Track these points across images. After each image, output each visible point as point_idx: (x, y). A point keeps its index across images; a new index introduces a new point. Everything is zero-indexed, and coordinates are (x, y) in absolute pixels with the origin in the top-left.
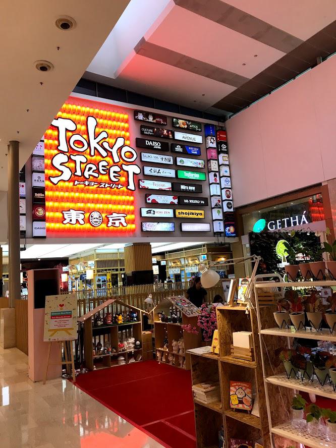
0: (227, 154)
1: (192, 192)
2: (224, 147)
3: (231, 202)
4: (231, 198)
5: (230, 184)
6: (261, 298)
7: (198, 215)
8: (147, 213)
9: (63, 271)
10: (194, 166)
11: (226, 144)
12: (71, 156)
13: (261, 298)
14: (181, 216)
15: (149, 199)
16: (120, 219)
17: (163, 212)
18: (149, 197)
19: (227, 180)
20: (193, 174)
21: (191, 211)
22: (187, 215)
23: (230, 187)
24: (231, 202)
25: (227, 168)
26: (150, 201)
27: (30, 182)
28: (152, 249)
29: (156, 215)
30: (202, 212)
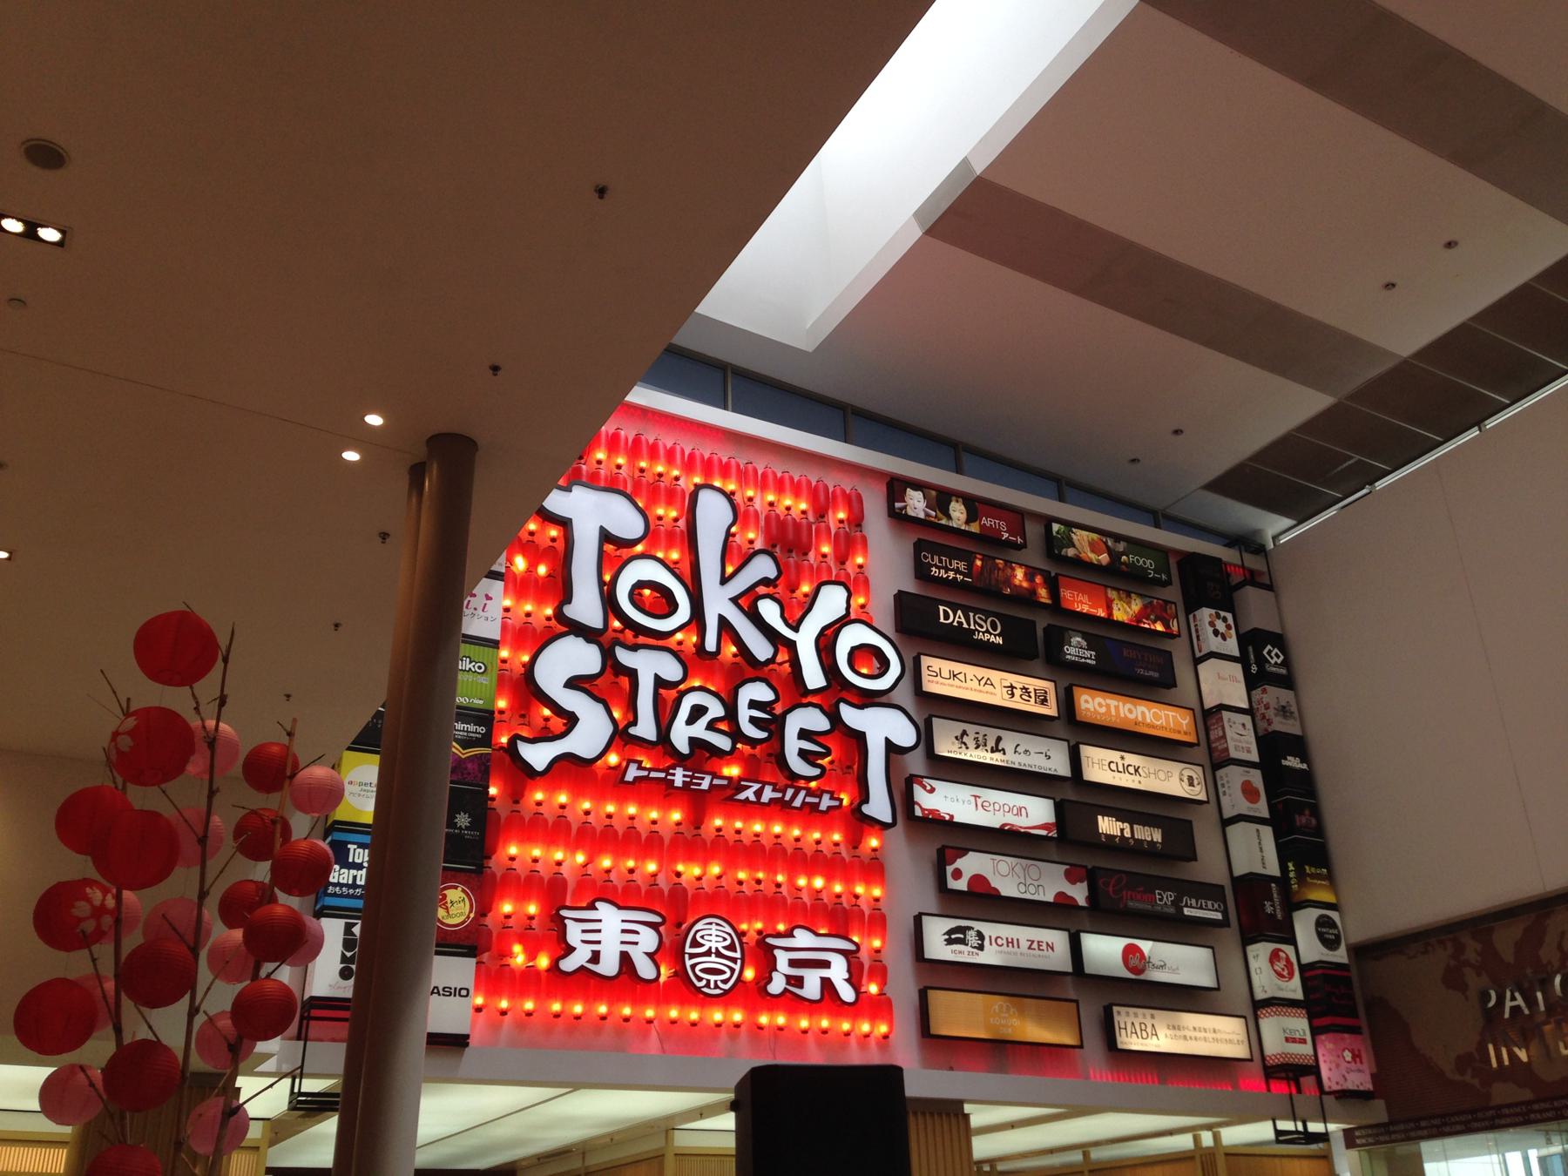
3: (1334, 915)
24: (1334, 915)
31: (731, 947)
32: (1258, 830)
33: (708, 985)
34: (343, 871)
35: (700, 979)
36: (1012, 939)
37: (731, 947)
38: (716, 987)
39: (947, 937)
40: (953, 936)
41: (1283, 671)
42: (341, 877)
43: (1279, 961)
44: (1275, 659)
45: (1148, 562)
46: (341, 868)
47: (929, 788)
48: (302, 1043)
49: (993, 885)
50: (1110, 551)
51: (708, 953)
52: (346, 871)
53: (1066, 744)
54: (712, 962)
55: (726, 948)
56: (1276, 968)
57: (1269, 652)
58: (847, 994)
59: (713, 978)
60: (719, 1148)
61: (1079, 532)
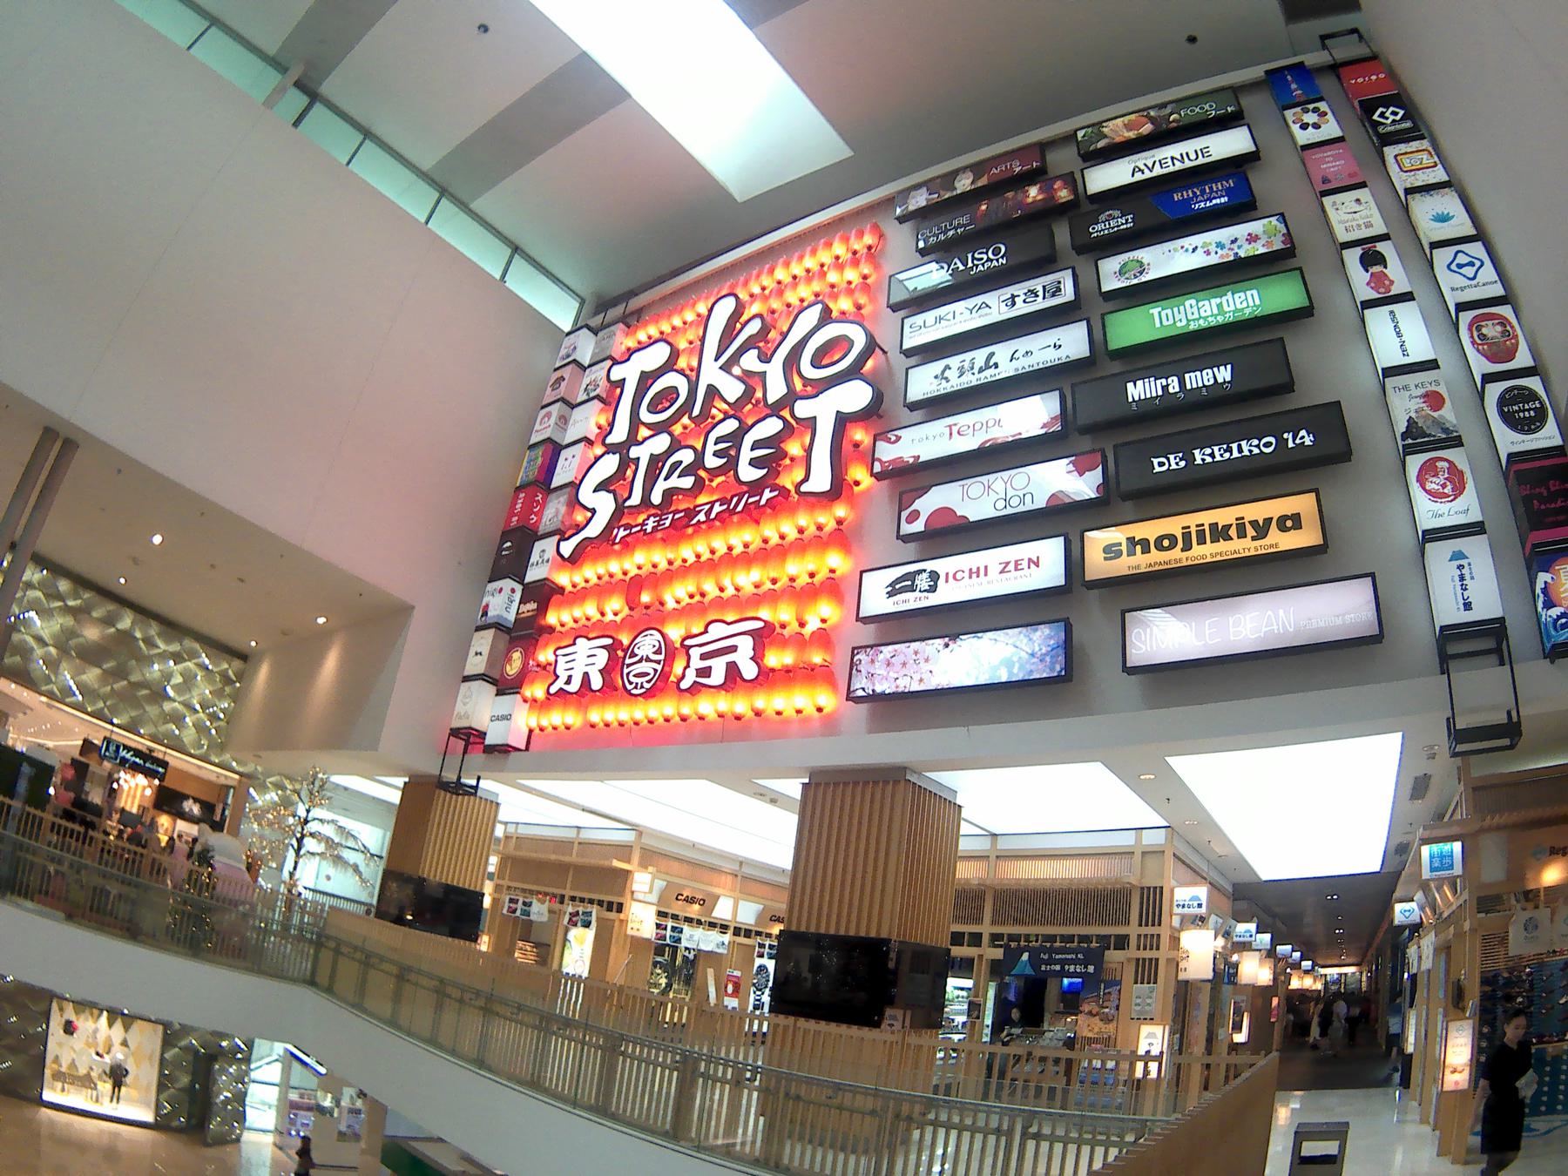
0: (1422, 137)
1: (1215, 399)
2: (1390, 117)
3: (1534, 383)
4: (1523, 359)
5: (1488, 273)
6: (1146, 981)
7: (1187, 536)
8: (890, 595)
9: (412, 886)
10: (1213, 260)
11: (1396, 100)
12: (609, 440)
13: (1146, 981)
14: (1127, 564)
15: (914, 516)
16: (733, 649)
17: (994, 570)
18: (917, 505)
19: (1462, 259)
20: (1215, 301)
21: (1206, 518)
22: (1176, 553)
23: (1498, 290)
24: (1534, 383)
25: (1449, 203)
26: (918, 526)
27: (914, 364)
28: (961, 840)
29: (948, 594)
30: (1303, 504)
31: (658, 652)
32: (1392, 312)
33: (636, 688)
34: (1200, 304)
35: (631, 683)
36: (978, 568)
37: (658, 652)
38: (642, 687)
39: (890, 589)
40: (897, 587)
41: (1408, 124)
42: (1202, 311)
43: (1436, 475)
44: (1392, 118)
45: (1207, 107)
46: (1197, 302)
47: (893, 438)
48: (1507, 667)
49: (959, 514)
50: (1152, 120)
51: (640, 661)
52: (1206, 302)
53: (1110, 319)
54: (645, 667)
55: (655, 653)
56: (1429, 486)
57: (1382, 115)
58: (749, 671)
59: (639, 680)
60: (973, 851)
61: (1110, 123)
